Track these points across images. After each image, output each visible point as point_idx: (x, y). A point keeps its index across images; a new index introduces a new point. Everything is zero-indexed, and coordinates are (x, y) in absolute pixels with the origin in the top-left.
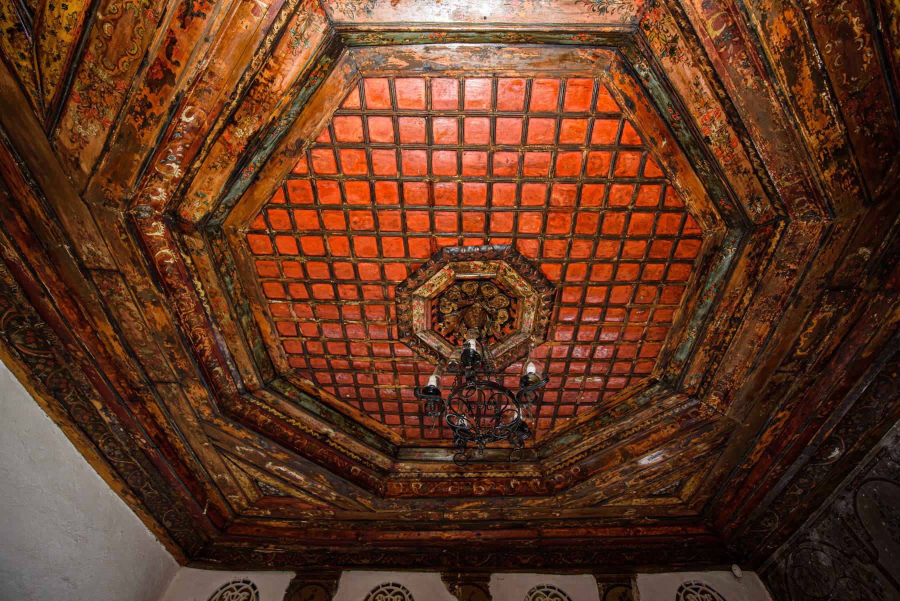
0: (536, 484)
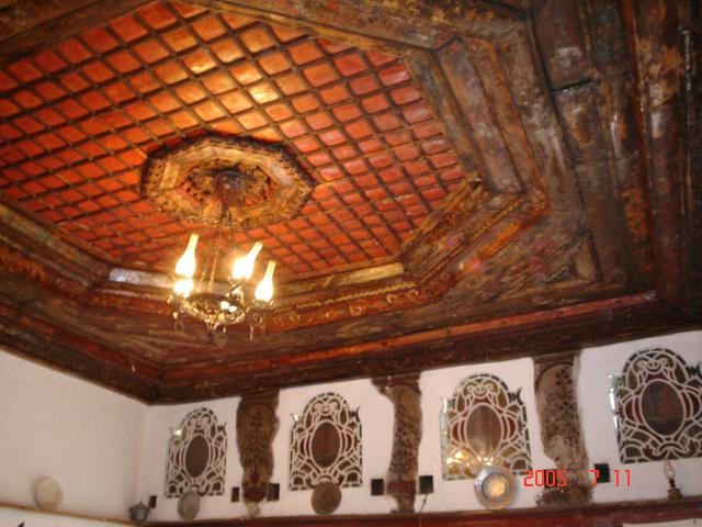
0: (414, 294)
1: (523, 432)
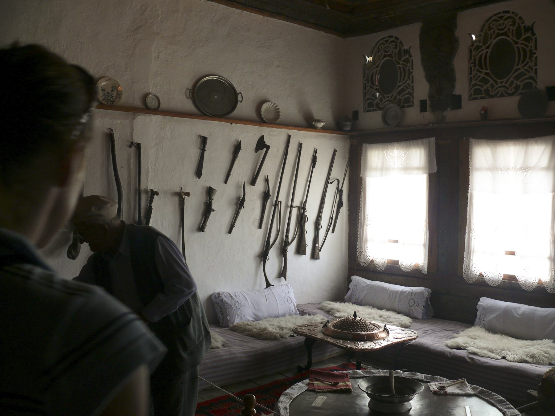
1: (533, 59)
